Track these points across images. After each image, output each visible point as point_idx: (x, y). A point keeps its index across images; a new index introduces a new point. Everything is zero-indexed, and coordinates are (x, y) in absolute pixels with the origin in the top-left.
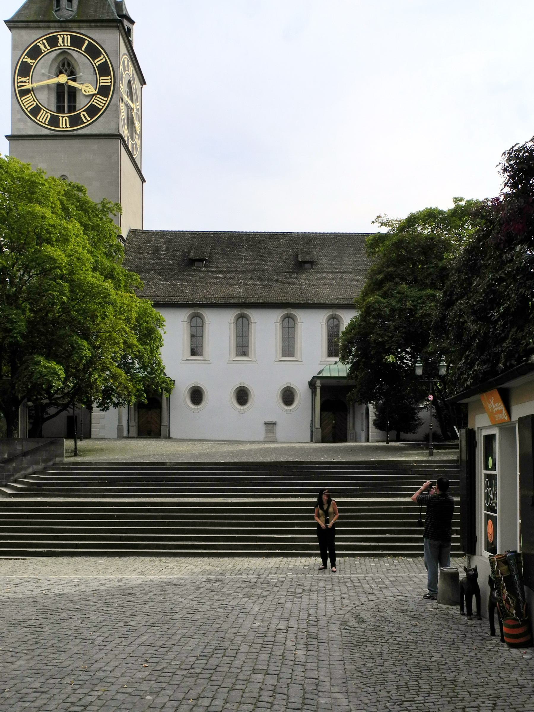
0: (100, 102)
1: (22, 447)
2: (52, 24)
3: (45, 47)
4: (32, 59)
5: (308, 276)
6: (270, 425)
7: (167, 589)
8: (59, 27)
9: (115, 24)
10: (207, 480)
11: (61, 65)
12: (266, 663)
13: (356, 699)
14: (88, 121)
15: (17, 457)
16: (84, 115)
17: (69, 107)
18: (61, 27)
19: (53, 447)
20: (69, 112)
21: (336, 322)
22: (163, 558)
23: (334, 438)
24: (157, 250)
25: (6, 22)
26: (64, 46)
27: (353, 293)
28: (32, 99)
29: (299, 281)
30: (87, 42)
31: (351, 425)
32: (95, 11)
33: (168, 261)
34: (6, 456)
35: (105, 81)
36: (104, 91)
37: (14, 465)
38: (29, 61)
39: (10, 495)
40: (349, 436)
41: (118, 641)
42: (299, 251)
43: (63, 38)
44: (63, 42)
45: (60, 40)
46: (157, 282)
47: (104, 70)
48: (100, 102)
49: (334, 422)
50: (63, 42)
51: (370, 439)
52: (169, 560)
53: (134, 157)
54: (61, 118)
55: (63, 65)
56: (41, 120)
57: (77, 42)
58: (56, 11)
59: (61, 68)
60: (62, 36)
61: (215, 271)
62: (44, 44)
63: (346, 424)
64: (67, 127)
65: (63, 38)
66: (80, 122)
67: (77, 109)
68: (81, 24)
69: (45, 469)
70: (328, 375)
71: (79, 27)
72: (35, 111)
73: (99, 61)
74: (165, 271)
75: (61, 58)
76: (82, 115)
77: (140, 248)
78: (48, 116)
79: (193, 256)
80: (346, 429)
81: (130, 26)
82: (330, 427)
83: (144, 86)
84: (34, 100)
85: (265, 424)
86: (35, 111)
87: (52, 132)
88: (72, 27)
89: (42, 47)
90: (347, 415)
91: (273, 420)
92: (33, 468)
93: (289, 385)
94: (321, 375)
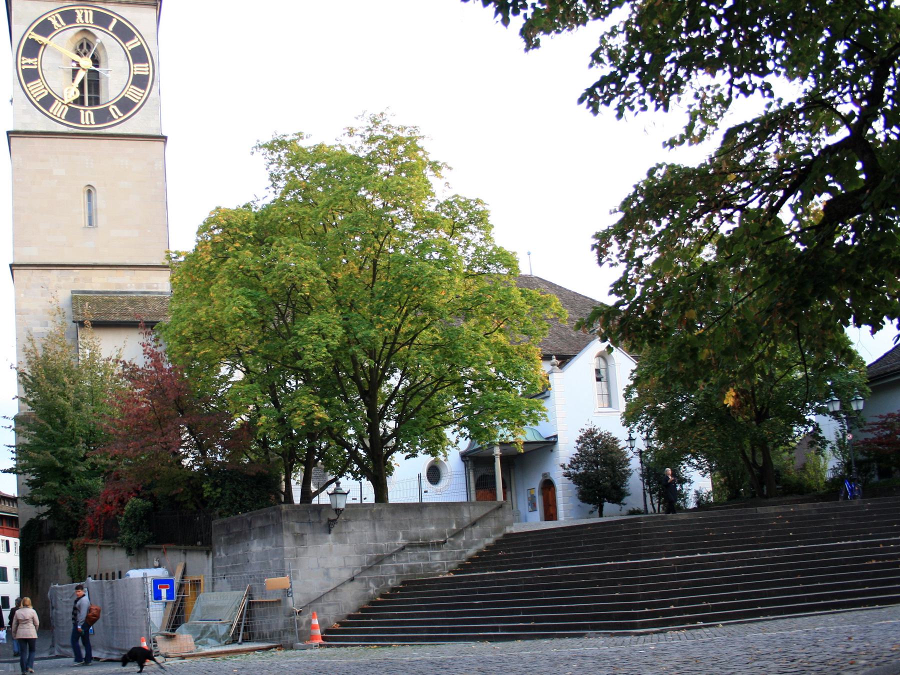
0: (133, 93)
1: (470, 514)
3: (59, 22)
10: (413, 616)
11: (78, 47)
15: (466, 527)
16: (113, 108)
19: (500, 513)
25: (527, 50)
26: (85, 23)
27: (816, 323)
28: (43, 87)
34: (454, 527)
35: (140, 69)
37: (464, 538)
43: (84, 14)
44: (83, 18)
45: (79, 16)
47: (139, 55)
48: (133, 93)
50: (83, 18)
55: (81, 46)
56: (55, 114)
59: (79, 50)
60: (82, 11)
62: (57, 19)
64: (91, 124)
65: (84, 14)
66: (108, 118)
67: (101, 103)
72: (47, 102)
73: (132, 45)
75: (80, 38)
78: (89, 114)
84: (45, 88)
86: (47, 102)
89: (55, 23)
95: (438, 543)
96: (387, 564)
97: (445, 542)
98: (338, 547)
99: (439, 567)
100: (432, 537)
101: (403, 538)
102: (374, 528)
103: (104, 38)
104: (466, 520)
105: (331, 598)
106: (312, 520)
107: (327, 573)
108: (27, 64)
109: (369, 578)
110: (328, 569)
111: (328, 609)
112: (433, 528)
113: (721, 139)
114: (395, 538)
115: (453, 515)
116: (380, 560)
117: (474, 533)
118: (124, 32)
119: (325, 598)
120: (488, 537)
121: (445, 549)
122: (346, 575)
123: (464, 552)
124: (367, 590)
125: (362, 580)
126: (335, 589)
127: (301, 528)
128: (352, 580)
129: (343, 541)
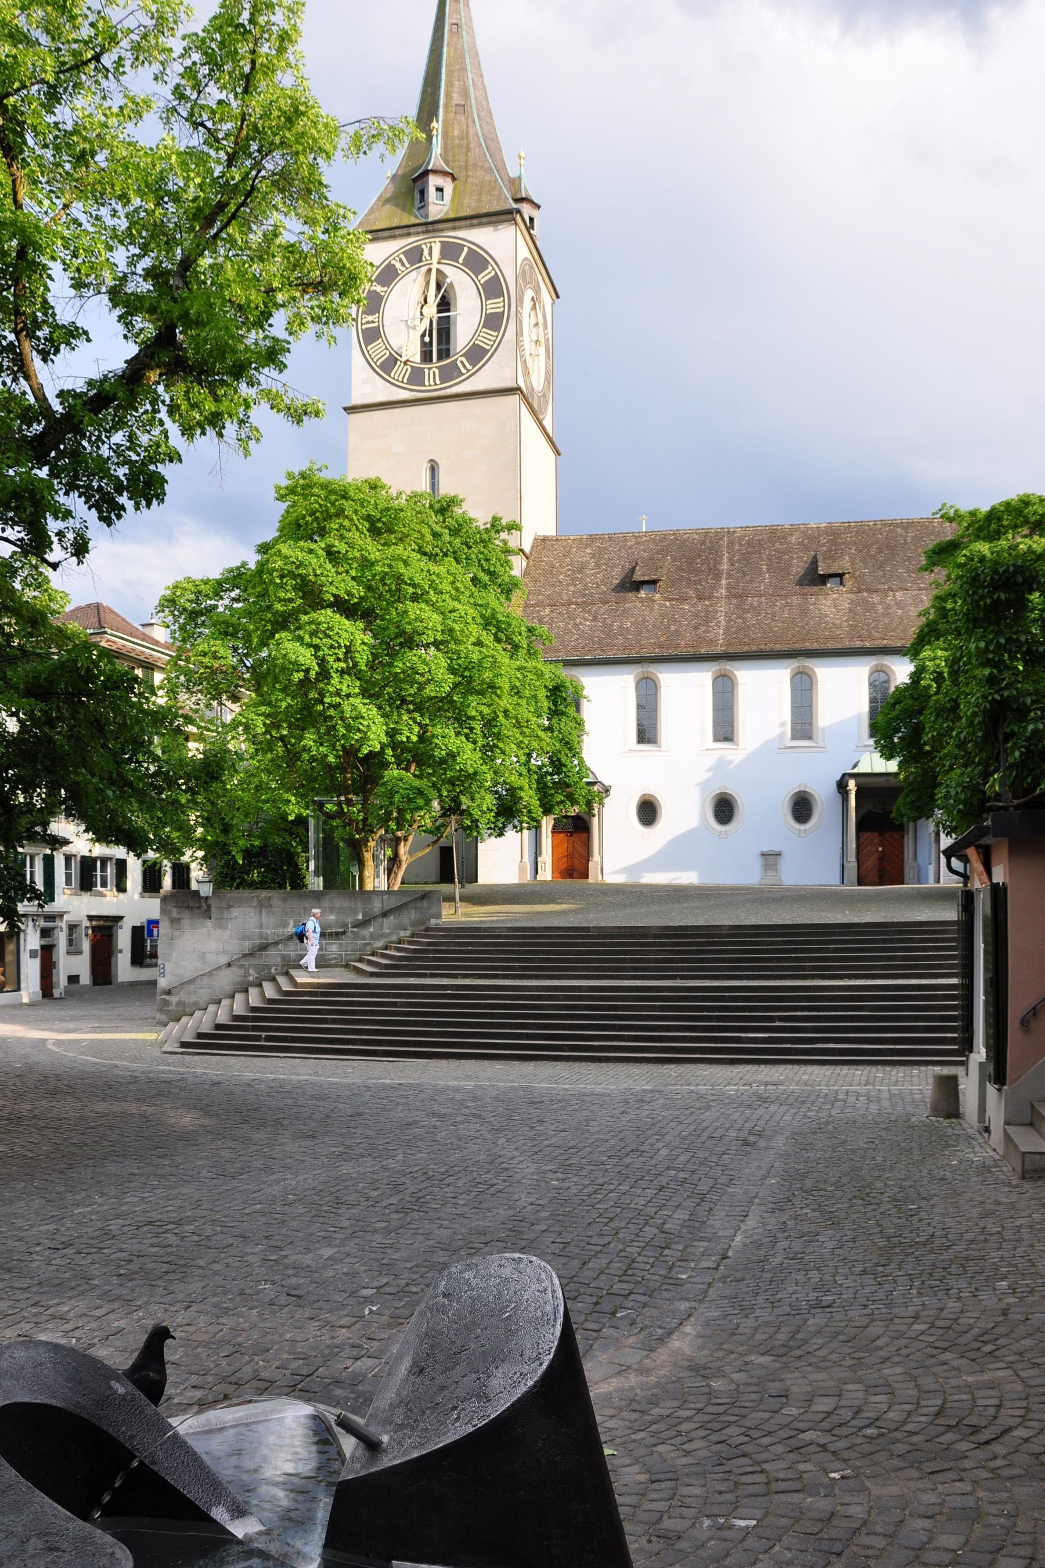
2: (412, 230)
3: (403, 265)
4: (383, 286)
5: (835, 599)
6: (771, 859)
7: (585, 1098)
8: (423, 233)
9: (509, 217)
12: (915, 1401)
13: (872, 1281)
14: (468, 371)
15: (375, 917)
16: (461, 360)
17: (439, 351)
18: (427, 232)
20: (440, 359)
21: (883, 677)
22: (584, 1064)
23: (880, 877)
24: (581, 569)
29: (819, 610)
30: (466, 250)
31: (911, 855)
32: (479, 201)
33: (598, 586)
34: (360, 917)
35: (495, 305)
36: (493, 322)
37: (372, 929)
38: (379, 289)
39: (372, 975)
40: (909, 872)
41: (523, 1142)
42: (820, 557)
46: (580, 623)
49: (880, 849)
51: (942, 878)
52: (592, 1066)
53: (541, 417)
54: (426, 371)
57: (450, 252)
58: (419, 208)
61: (677, 600)
62: (401, 261)
63: (902, 853)
64: (436, 384)
65: (431, 248)
67: (452, 353)
68: (457, 224)
69: (412, 936)
70: (868, 770)
71: (455, 229)
72: (389, 364)
73: (485, 276)
74: (593, 604)
76: (458, 363)
77: (553, 567)
79: (638, 576)
80: (902, 860)
81: (534, 213)
82: (876, 856)
83: (557, 301)
84: (386, 348)
85: (763, 855)
87: (413, 393)
88: (442, 230)
89: (398, 265)
90: (903, 837)
91: (776, 848)
92: (398, 934)
93: (802, 788)
94: (855, 771)
95: (337, 934)
96: (272, 952)
97: (344, 933)
98: (217, 933)
99: (335, 958)
100: (330, 926)
101: (294, 926)
102: (261, 914)
103: (458, 277)
104: (376, 910)
105: (205, 981)
106: (191, 905)
107: (203, 956)
108: (368, 322)
109: (250, 965)
110: (204, 953)
111: (200, 992)
112: (333, 917)
113: (47, 395)
114: (285, 925)
115: (359, 905)
116: (263, 947)
117: (385, 924)
118: (477, 262)
119: (198, 980)
120: (405, 929)
121: (344, 940)
122: (224, 960)
123: (369, 944)
124: (245, 977)
125: (241, 966)
126: (210, 974)
127: (178, 913)
128: (229, 965)
129: (222, 927)
